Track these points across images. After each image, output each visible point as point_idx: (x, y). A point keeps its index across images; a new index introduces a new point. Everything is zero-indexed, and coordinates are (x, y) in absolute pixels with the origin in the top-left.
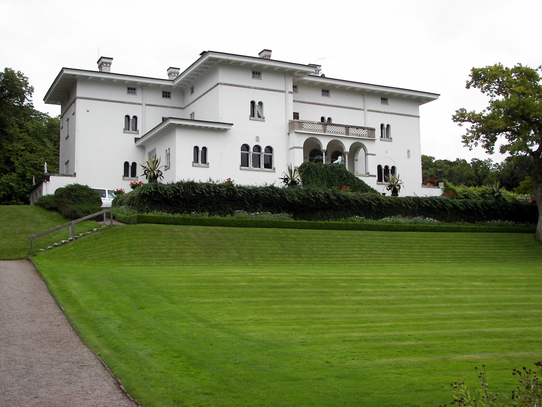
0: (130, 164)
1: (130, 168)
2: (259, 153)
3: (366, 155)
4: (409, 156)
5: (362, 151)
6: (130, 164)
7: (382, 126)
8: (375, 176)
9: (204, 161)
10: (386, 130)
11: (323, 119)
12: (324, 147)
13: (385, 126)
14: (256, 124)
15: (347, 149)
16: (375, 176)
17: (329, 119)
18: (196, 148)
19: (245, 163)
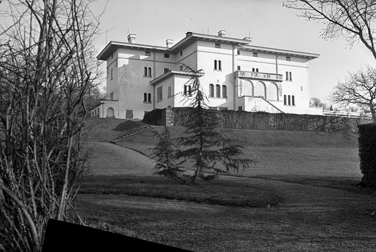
14: (217, 72)
17: (257, 69)
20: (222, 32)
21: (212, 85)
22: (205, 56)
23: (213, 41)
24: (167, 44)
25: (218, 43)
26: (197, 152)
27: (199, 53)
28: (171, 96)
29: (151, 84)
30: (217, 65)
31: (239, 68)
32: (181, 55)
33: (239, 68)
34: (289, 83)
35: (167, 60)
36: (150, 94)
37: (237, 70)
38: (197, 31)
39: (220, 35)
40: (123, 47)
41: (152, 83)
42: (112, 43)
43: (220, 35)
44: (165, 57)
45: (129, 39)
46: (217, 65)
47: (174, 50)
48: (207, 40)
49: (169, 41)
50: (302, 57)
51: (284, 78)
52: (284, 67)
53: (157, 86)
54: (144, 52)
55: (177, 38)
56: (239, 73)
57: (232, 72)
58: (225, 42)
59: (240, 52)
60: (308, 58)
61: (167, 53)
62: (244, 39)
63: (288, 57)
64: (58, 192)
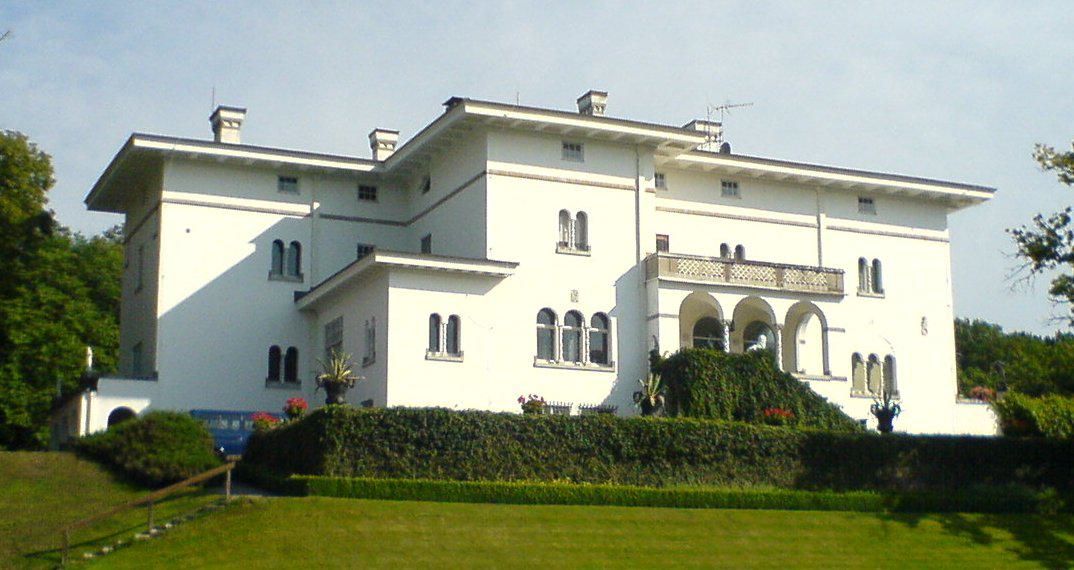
0: (284, 352)
1: (283, 361)
2: (604, 331)
3: (825, 330)
4: (924, 331)
5: (814, 320)
6: (284, 352)
7: (862, 262)
8: (845, 380)
9: (877, 288)
10: (872, 276)
11: (724, 248)
12: (728, 315)
13: (870, 264)
14: (573, 262)
15: (780, 319)
16: (845, 380)
17: (739, 249)
18: (435, 319)
19: (546, 346)
20: (595, 99)
21: (547, 315)
22: (518, 202)
23: (552, 132)
24: (374, 145)
25: (573, 146)
26: (1032, 374)
27: (491, 180)
28: (374, 356)
29: (302, 311)
30: (576, 232)
31: (663, 243)
32: (427, 188)
33: (663, 243)
34: (871, 303)
35: (366, 209)
36: (293, 352)
37: (653, 250)
38: (491, 90)
39: (586, 110)
40: (183, 159)
41: (305, 302)
42: (138, 143)
43: (586, 110)
44: (361, 197)
45: (217, 124)
46: (576, 232)
47: (396, 170)
48: (528, 130)
49: (380, 136)
50: (924, 199)
51: (851, 281)
52: (844, 243)
53: (327, 318)
54: (274, 182)
55: (408, 119)
56: (662, 263)
57: (635, 263)
58: (604, 140)
59: (668, 180)
60: (947, 203)
61: (367, 188)
62: (688, 129)
63: (867, 201)
64: (627, 446)
